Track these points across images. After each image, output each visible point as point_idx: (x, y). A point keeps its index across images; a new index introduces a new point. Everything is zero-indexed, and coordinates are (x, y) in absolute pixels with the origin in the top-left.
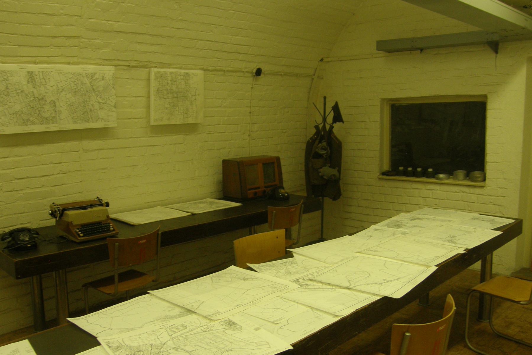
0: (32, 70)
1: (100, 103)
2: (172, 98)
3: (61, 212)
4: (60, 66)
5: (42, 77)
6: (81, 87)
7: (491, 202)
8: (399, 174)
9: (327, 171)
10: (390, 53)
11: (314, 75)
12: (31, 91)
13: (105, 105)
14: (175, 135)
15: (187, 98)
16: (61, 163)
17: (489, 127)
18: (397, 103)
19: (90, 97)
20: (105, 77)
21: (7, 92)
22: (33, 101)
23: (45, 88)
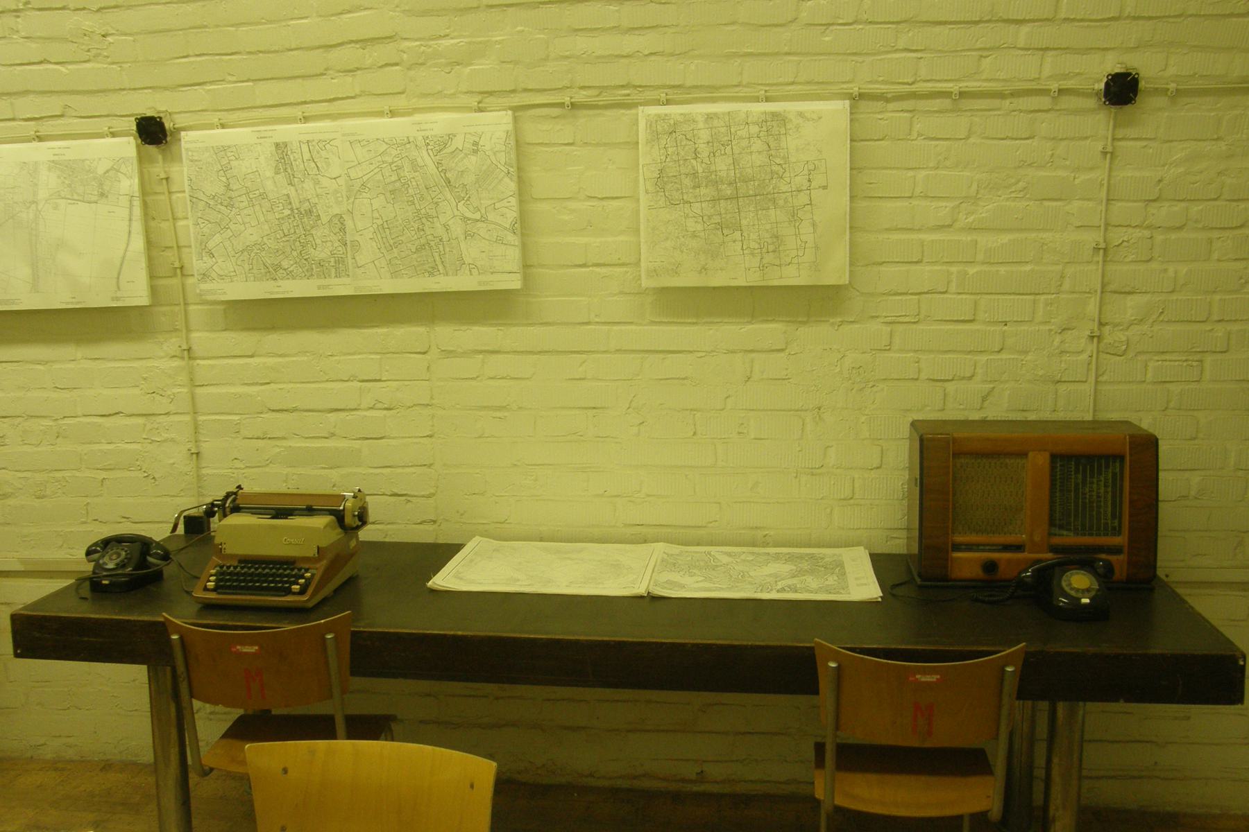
0: (284, 141)
1: (465, 219)
5: (307, 156)
6: (411, 176)
12: (285, 192)
13: (485, 225)
14: (750, 323)
15: (774, 201)
16: (380, 380)
17: (29, 283)
19: (437, 203)
20: (481, 143)
21: (229, 198)
22: (290, 218)
23: (317, 182)
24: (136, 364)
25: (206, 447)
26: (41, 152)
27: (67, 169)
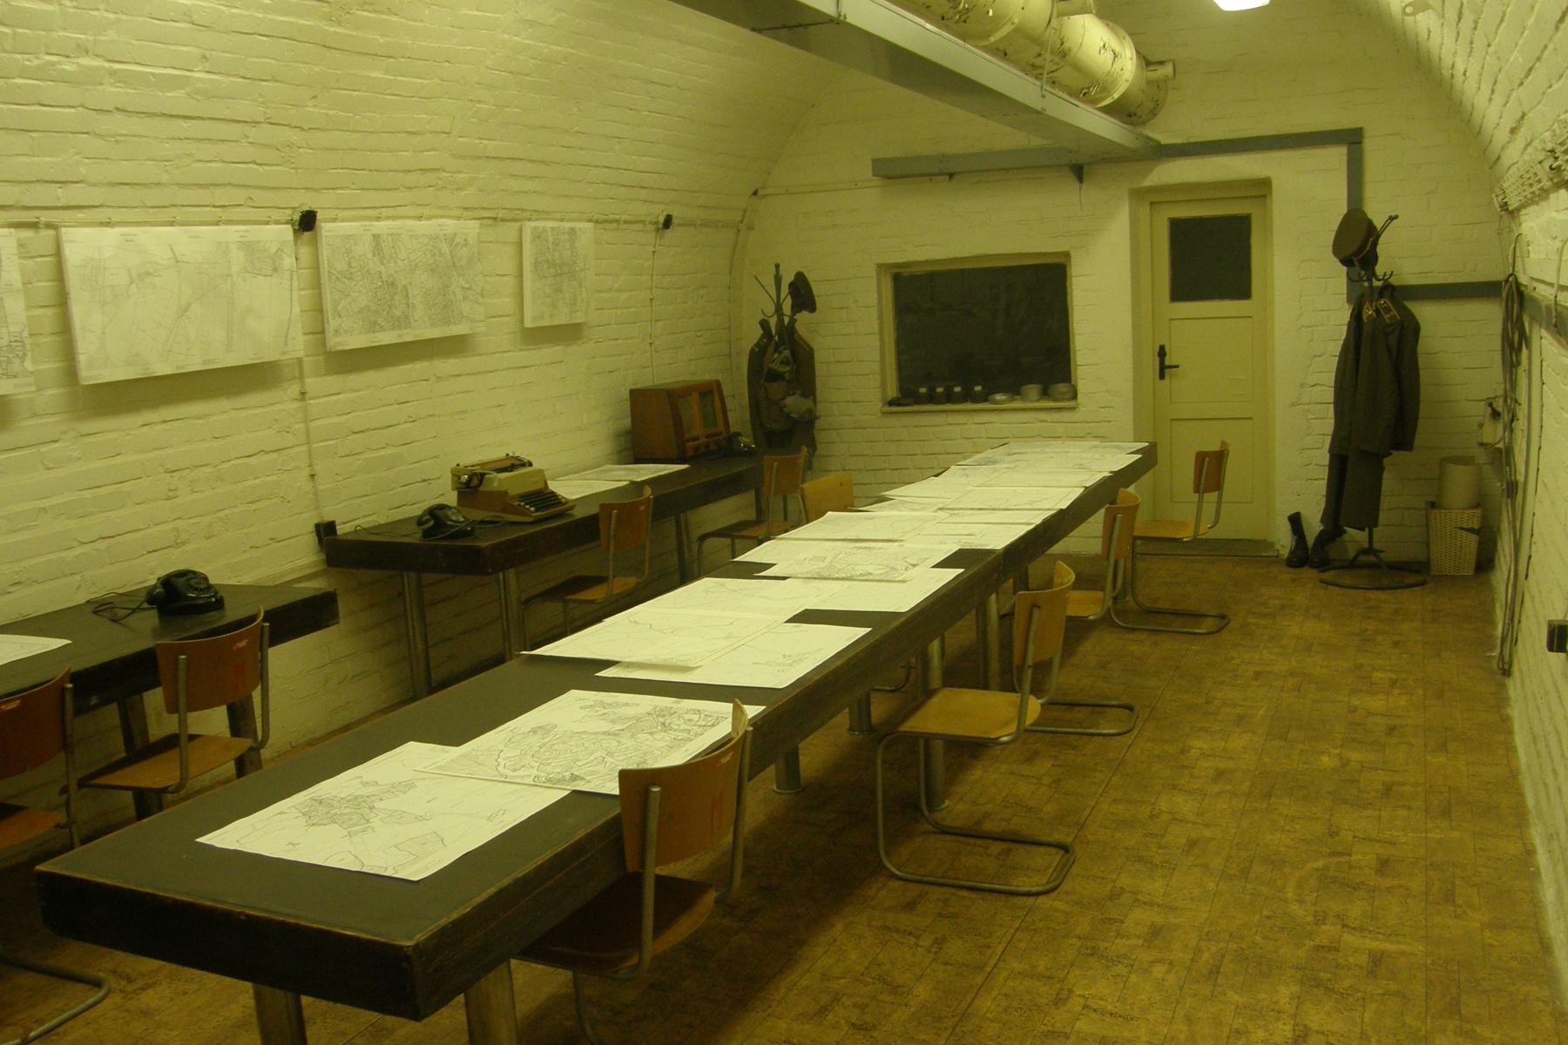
1: (463, 288)
2: (554, 276)
3: (480, 477)
7: (1089, 434)
8: (919, 400)
9: (794, 403)
10: (891, 181)
11: (742, 222)
16: (408, 402)
18: (906, 272)
23: (396, 262)
24: (268, 409)
25: (318, 468)
26: (233, 233)
27: (249, 247)
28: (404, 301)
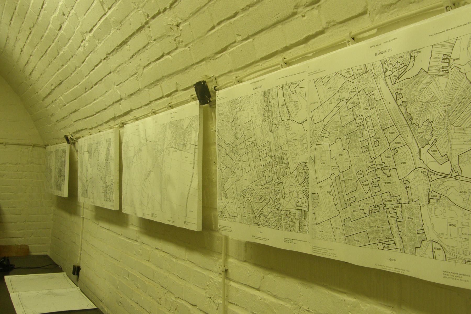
1: (429, 173)
4: (160, 101)
13: (455, 183)
23: (288, 128)
28: (300, 188)
